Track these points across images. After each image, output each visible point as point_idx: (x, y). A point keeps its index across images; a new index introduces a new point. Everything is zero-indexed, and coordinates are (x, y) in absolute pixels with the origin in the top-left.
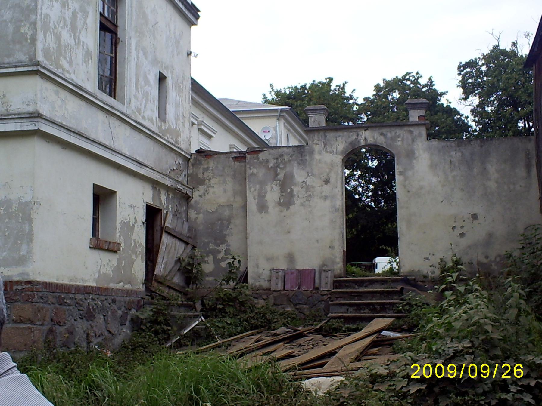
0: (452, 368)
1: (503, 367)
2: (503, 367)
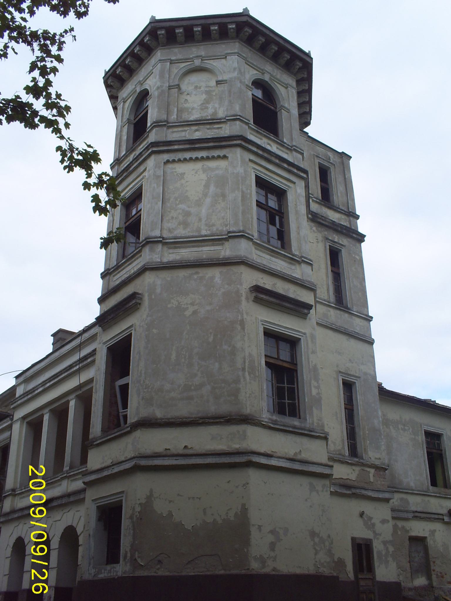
0: (42, 550)
1: (44, 570)
2: (44, 570)
